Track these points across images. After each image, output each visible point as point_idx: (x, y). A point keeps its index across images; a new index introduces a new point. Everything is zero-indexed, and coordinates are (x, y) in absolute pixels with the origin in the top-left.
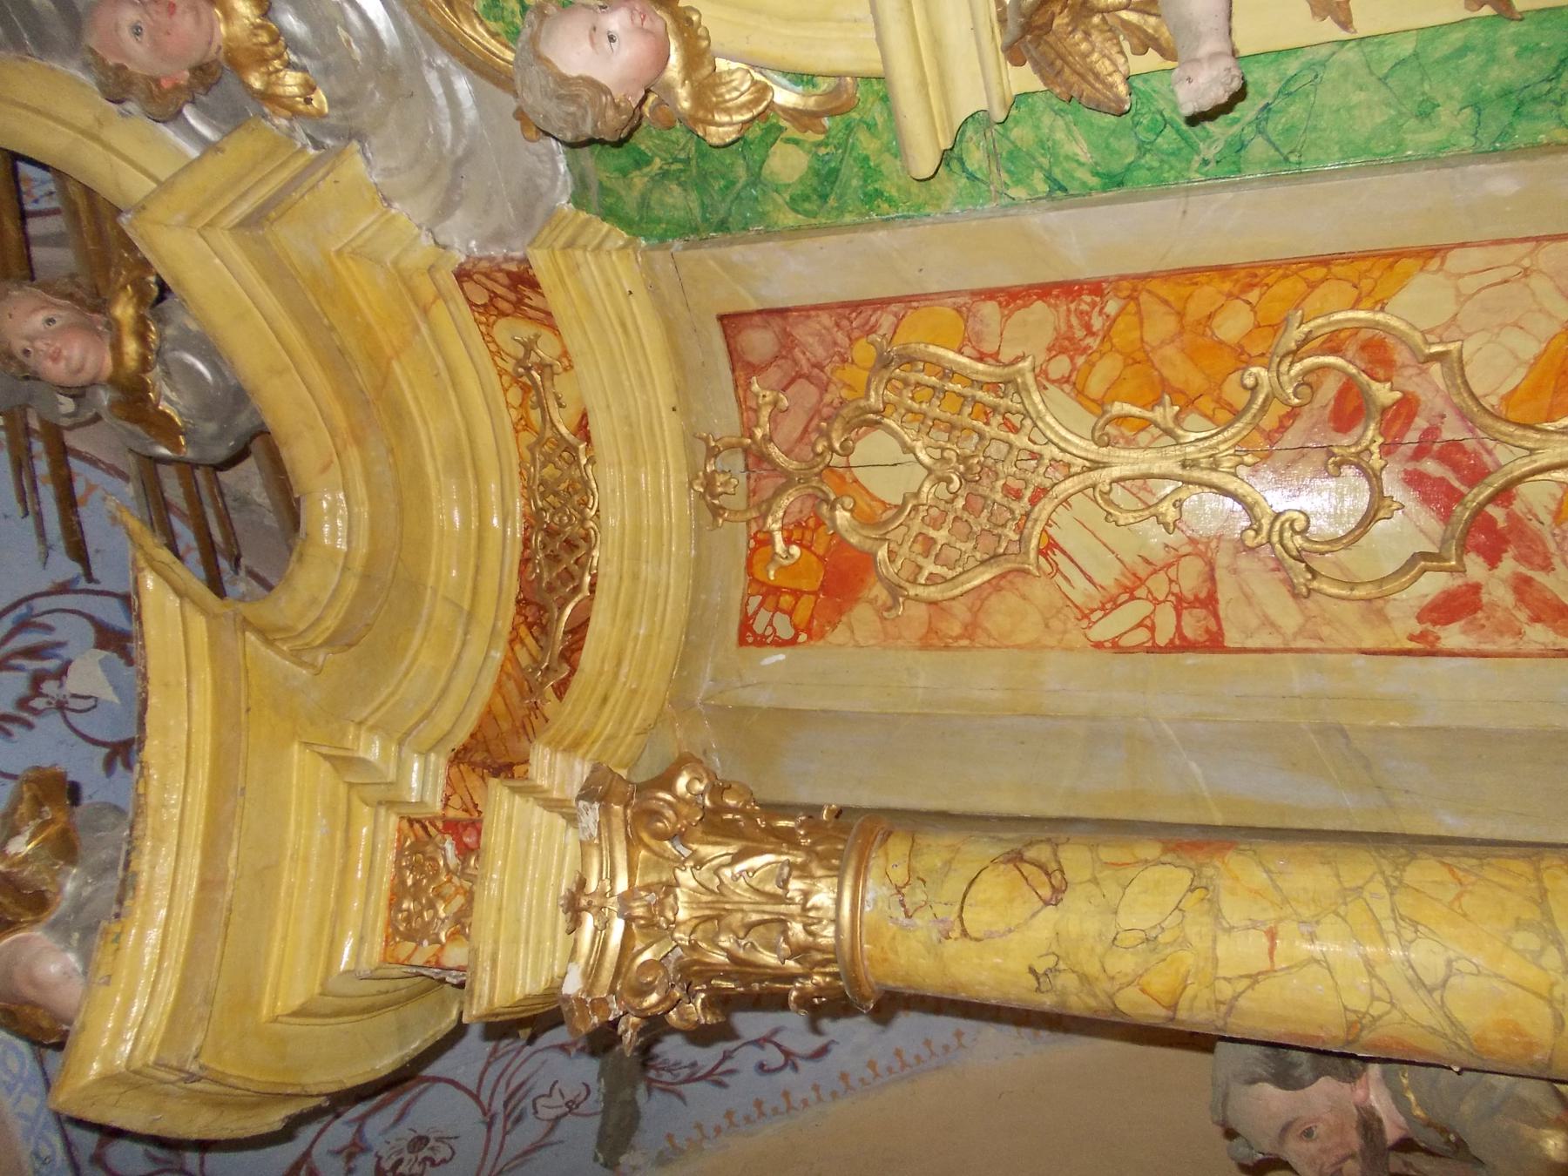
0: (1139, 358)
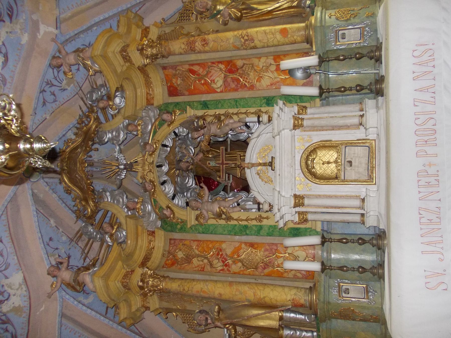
0: (203, 248)
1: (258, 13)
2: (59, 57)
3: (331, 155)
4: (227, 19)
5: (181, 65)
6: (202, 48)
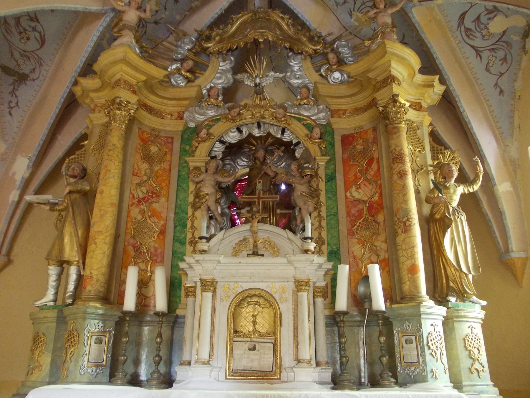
0: (162, 176)
3: (263, 325)
5: (378, 148)
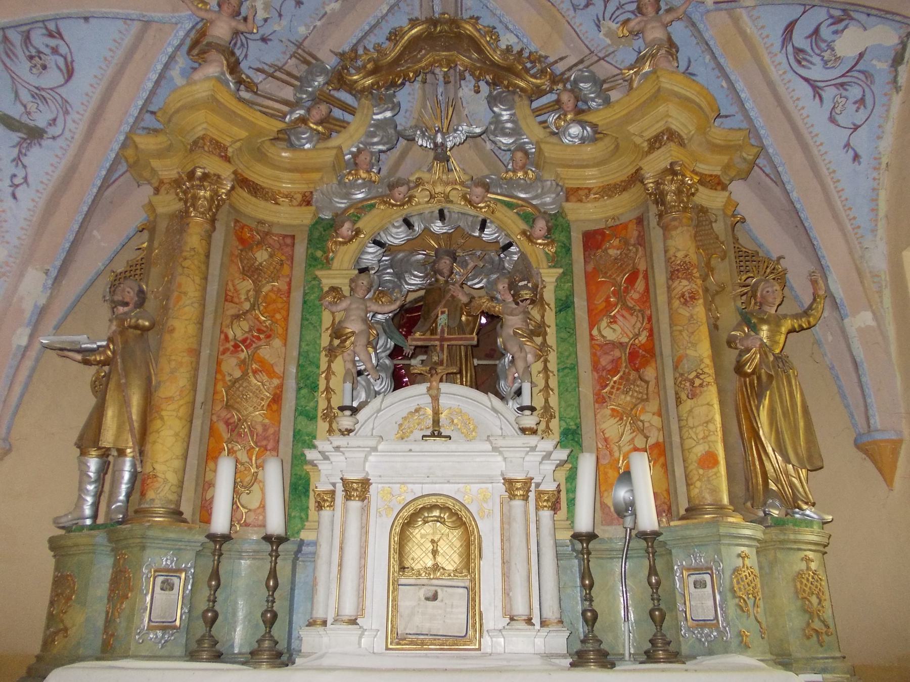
0: (274, 301)
1: (754, 408)
2: (658, 9)
3: (450, 558)
4: (738, 345)
6: (677, 294)
